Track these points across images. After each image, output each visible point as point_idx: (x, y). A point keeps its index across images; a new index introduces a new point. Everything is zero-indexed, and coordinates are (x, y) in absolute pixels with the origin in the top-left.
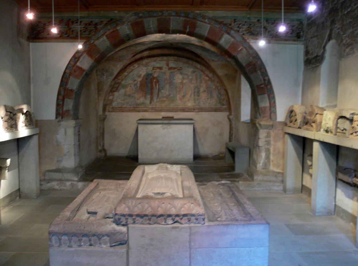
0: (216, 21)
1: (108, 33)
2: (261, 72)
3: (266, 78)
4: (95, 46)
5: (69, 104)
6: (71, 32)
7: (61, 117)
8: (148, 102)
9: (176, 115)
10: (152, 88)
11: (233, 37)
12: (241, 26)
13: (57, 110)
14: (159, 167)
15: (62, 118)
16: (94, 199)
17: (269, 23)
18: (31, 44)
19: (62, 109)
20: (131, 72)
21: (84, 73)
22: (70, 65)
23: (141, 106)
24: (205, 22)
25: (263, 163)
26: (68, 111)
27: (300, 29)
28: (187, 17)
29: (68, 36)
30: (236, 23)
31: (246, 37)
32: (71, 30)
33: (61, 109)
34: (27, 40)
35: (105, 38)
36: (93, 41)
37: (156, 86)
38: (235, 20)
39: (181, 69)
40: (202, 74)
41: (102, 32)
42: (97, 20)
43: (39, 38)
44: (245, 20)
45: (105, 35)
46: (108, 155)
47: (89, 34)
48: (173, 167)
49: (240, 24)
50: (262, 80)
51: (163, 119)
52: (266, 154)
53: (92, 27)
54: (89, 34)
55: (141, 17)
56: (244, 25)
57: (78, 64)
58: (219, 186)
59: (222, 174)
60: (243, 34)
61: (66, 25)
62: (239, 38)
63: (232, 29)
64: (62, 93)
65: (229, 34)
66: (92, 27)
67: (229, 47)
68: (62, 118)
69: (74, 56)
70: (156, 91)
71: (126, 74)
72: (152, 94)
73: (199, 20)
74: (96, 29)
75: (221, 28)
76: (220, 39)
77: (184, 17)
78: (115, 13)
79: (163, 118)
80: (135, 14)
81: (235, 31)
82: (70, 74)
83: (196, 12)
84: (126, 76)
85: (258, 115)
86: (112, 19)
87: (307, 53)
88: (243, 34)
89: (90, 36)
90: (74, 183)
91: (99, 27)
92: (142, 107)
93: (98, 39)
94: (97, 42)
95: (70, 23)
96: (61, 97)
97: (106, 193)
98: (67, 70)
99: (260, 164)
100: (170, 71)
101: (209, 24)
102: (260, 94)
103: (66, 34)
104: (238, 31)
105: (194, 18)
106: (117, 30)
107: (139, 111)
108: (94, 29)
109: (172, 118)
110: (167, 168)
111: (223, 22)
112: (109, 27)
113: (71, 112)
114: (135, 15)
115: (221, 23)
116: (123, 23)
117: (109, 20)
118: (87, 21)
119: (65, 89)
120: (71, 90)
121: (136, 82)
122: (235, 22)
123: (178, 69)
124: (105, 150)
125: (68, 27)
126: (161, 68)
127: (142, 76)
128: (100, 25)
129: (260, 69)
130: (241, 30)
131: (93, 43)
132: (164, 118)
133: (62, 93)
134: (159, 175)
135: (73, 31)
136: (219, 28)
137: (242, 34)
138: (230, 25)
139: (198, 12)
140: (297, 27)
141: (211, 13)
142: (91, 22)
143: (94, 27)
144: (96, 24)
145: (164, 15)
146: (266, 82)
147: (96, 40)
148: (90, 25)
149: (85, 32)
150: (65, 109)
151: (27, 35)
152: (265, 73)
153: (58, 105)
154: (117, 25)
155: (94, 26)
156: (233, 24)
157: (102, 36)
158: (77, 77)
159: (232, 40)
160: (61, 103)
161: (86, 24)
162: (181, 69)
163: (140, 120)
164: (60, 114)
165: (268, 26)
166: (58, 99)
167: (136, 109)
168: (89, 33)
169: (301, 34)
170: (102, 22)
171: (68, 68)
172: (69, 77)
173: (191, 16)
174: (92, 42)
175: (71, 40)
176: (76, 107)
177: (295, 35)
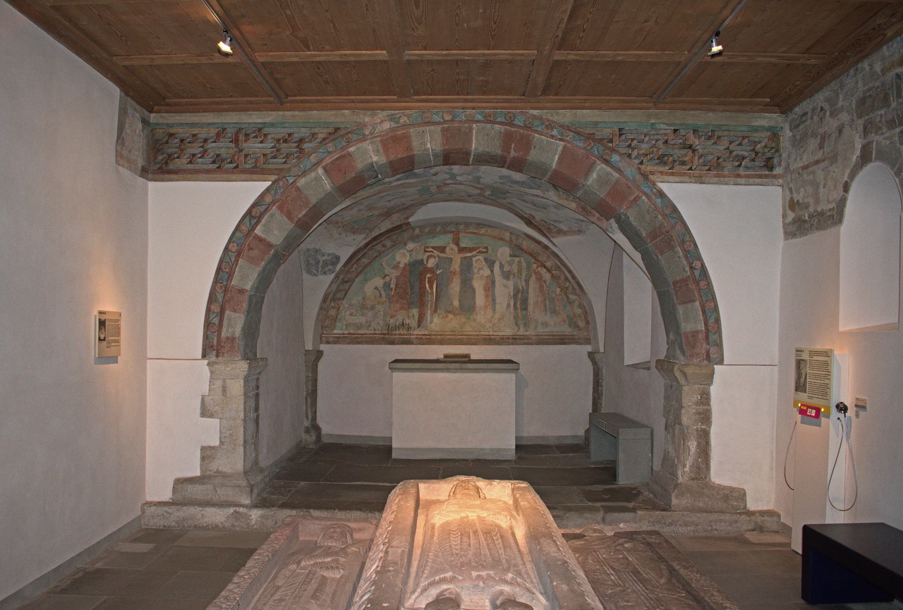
0: (578, 133)
1: (328, 160)
2: (684, 250)
3: (697, 264)
4: (298, 189)
5: (235, 324)
6: (242, 158)
7: (214, 353)
8: (414, 323)
9: (476, 352)
10: (422, 293)
11: (618, 170)
12: (635, 142)
13: (206, 337)
14: (456, 486)
15: (217, 356)
16: (279, 587)
17: (700, 137)
18: (152, 185)
19: (219, 335)
20: (377, 257)
21: (272, 252)
22: (238, 234)
23: (397, 332)
24: (552, 137)
25: (691, 466)
26: (232, 339)
27: (773, 151)
28: (511, 124)
29: (237, 167)
30: (623, 137)
31: (648, 168)
32: (244, 153)
33: (216, 334)
34: (141, 176)
35: (320, 171)
36: (294, 178)
37: (431, 288)
38: (620, 130)
39: (485, 250)
40: (533, 260)
41: (313, 159)
42: (304, 132)
43: (170, 172)
44: (645, 131)
45: (324, 164)
46: (325, 440)
47: (285, 163)
48: (491, 484)
49: (632, 140)
50: (687, 269)
51: (446, 359)
52: (698, 445)
53: (291, 147)
54: (285, 163)
55: (405, 125)
56: (642, 141)
57: (258, 231)
58: (621, 541)
59: (590, 488)
60: (641, 163)
61: (231, 142)
62: (630, 171)
63: (613, 150)
64: (220, 297)
65: (607, 162)
66: (291, 147)
67: (608, 194)
68: (217, 356)
69: (249, 212)
70: (431, 298)
71: (365, 261)
72: (422, 305)
73: (537, 132)
74: (301, 151)
75: (589, 148)
76: (587, 174)
77: (501, 123)
78: (345, 117)
79: (446, 356)
80: (392, 118)
81: (621, 155)
82: (239, 254)
83: (531, 111)
84: (366, 267)
85: (678, 352)
86: (337, 129)
87: (793, 205)
88: (641, 163)
89: (285, 166)
90: (241, 510)
91: (306, 146)
92: (400, 334)
93: (305, 173)
94: (301, 182)
95: (241, 137)
96: (216, 308)
97: (313, 565)
98: (231, 245)
99: (684, 466)
100: (462, 255)
101: (561, 140)
102: (684, 303)
103: (231, 162)
104: (629, 156)
105: (526, 127)
106: (349, 154)
107: (392, 343)
108: (295, 150)
109: (465, 359)
110: (478, 489)
111: (593, 134)
112: (330, 147)
113: (240, 343)
114: (391, 120)
115: (590, 137)
116: (364, 139)
117: (331, 130)
118: (282, 132)
119: (226, 290)
120: (241, 291)
121: (388, 278)
122: (620, 135)
123: (478, 251)
124: (317, 429)
125: (237, 146)
126: (442, 249)
127: (402, 265)
128: (310, 142)
129: (683, 243)
130: (635, 153)
131: (292, 183)
132: (449, 359)
133: (220, 297)
134: (463, 515)
135: (246, 156)
136: (585, 148)
137: (637, 161)
138: (611, 141)
139: (536, 112)
140: (766, 146)
141: (565, 116)
142: (290, 135)
143: (298, 147)
144: (301, 141)
145: (457, 119)
146: (697, 273)
147: (299, 176)
148: (286, 141)
149: (275, 157)
150: (224, 334)
151: (140, 163)
152: (693, 254)
153: (208, 324)
154: (349, 143)
155: (296, 145)
156: (616, 139)
157: (315, 167)
158: (253, 261)
159: (616, 175)
160: (216, 321)
161: (278, 140)
162: (485, 250)
163: (396, 361)
164: (212, 347)
165: (697, 142)
166: (208, 310)
167: (386, 338)
168: (285, 160)
169: (776, 161)
170: (313, 135)
171: (234, 239)
172: (237, 261)
173: (520, 121)
174: (291, 180)
175: (243, 176)
176: (251, 332)
177: (763, 164)
